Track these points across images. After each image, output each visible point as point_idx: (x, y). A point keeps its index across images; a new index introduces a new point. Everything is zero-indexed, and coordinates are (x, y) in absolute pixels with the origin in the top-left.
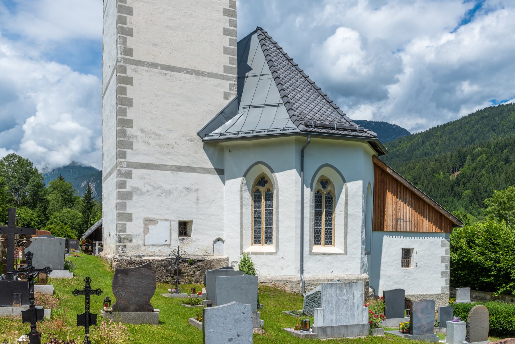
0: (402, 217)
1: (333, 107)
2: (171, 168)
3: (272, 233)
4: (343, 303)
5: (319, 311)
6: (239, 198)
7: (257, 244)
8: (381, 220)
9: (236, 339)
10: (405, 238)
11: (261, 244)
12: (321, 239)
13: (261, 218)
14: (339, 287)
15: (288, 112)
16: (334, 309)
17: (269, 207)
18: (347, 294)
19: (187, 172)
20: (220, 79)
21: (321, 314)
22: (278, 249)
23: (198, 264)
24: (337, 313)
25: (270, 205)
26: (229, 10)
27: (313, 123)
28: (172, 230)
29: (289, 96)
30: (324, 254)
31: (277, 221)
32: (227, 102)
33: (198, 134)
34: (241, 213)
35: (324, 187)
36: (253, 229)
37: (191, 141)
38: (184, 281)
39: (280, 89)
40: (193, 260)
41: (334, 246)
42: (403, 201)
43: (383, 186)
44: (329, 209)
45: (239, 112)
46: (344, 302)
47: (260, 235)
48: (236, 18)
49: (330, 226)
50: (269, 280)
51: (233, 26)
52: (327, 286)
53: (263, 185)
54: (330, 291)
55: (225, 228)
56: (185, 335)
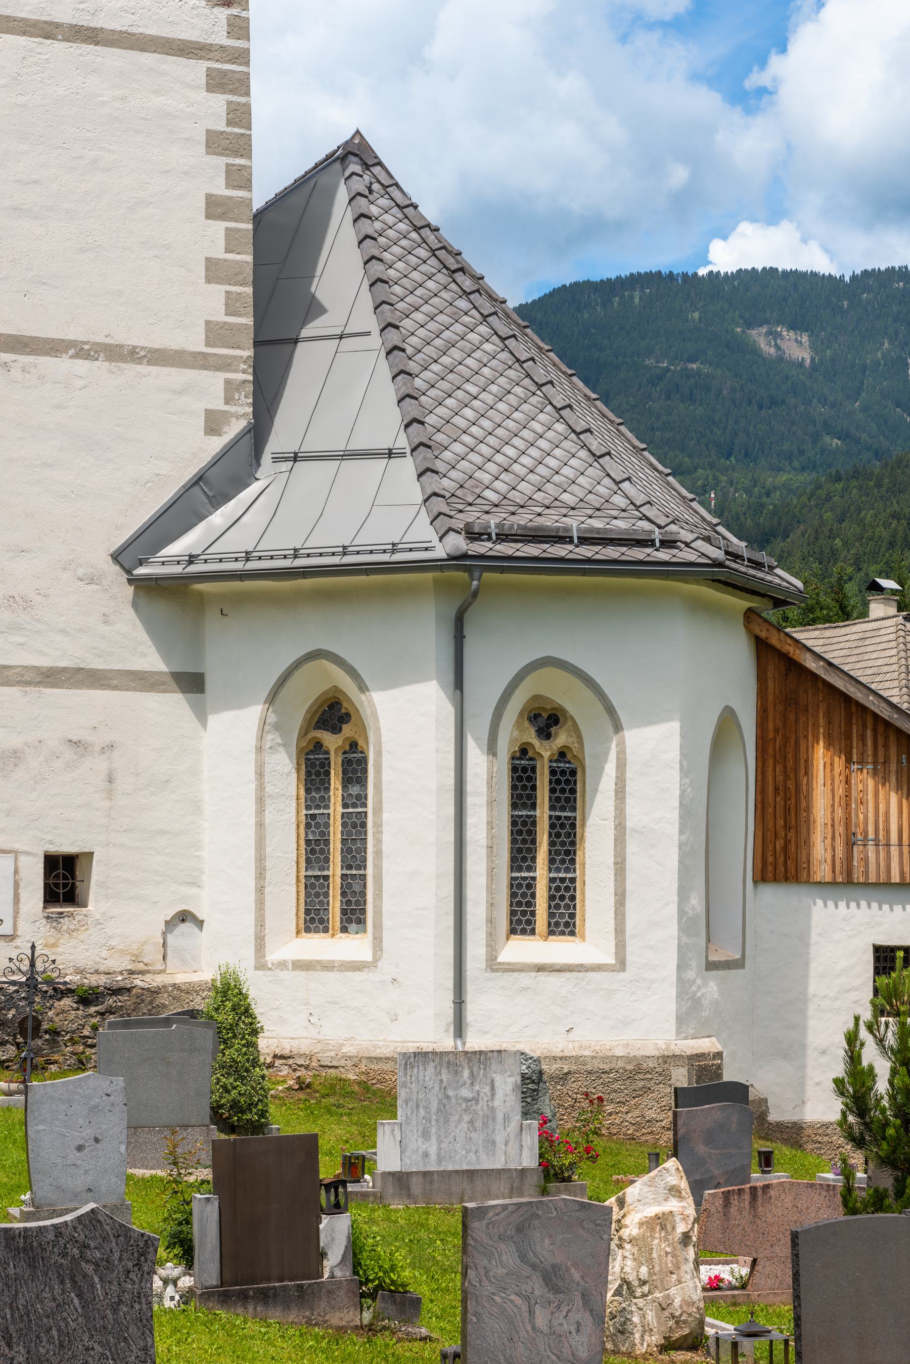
0: (871, 829)
1: (590, 451)
2: (22, 676)
3: (363, 894)
4: (459, 1109)
5: (388, 1128)
6: (252, 775)
7: (317, 931)
8: (787, 842)
9: (92, 1148)
10: (886, 907)
11: (327, 932)
12: (533, 913)
13: (327, 842)
14: (448, 1063)
15: (423, 478)
16: (433, 1123)
17: (354, 805)
18: (472, 1084)
19: (76, 687)
20: (193, 368)
21: (394, 1136)
22: (381, 950)
23: (110, 1001)
24: (442, 1135)
25: (358, 797)
26: (227, 133)
27: (493, 526)
28: (22, 885)
29: (430, 419)
30: (540, 968)
31: (379, 853)
32: (217, 444)
33: (116, 557)
34: (260, 825)
35: (545, 733)
36: (303, 880)
37: (91, 581)
38: (61, 1059)
39: (404, 391)
40: (91, 988)
41: (583, 938)
42: (875, 773)
43: (792, 717)
44: (563, 809)
45: (257, 476)
46: (464, 1106)
47: (325, 900)
48: (250, 158)
49: (567, 870)
50: (350, 1057)
51: (240, 187)
52: (412, 1059)
53: (336, 730)
54: (421, 1074)
55: (204, 878)
56: (15, 1174)
